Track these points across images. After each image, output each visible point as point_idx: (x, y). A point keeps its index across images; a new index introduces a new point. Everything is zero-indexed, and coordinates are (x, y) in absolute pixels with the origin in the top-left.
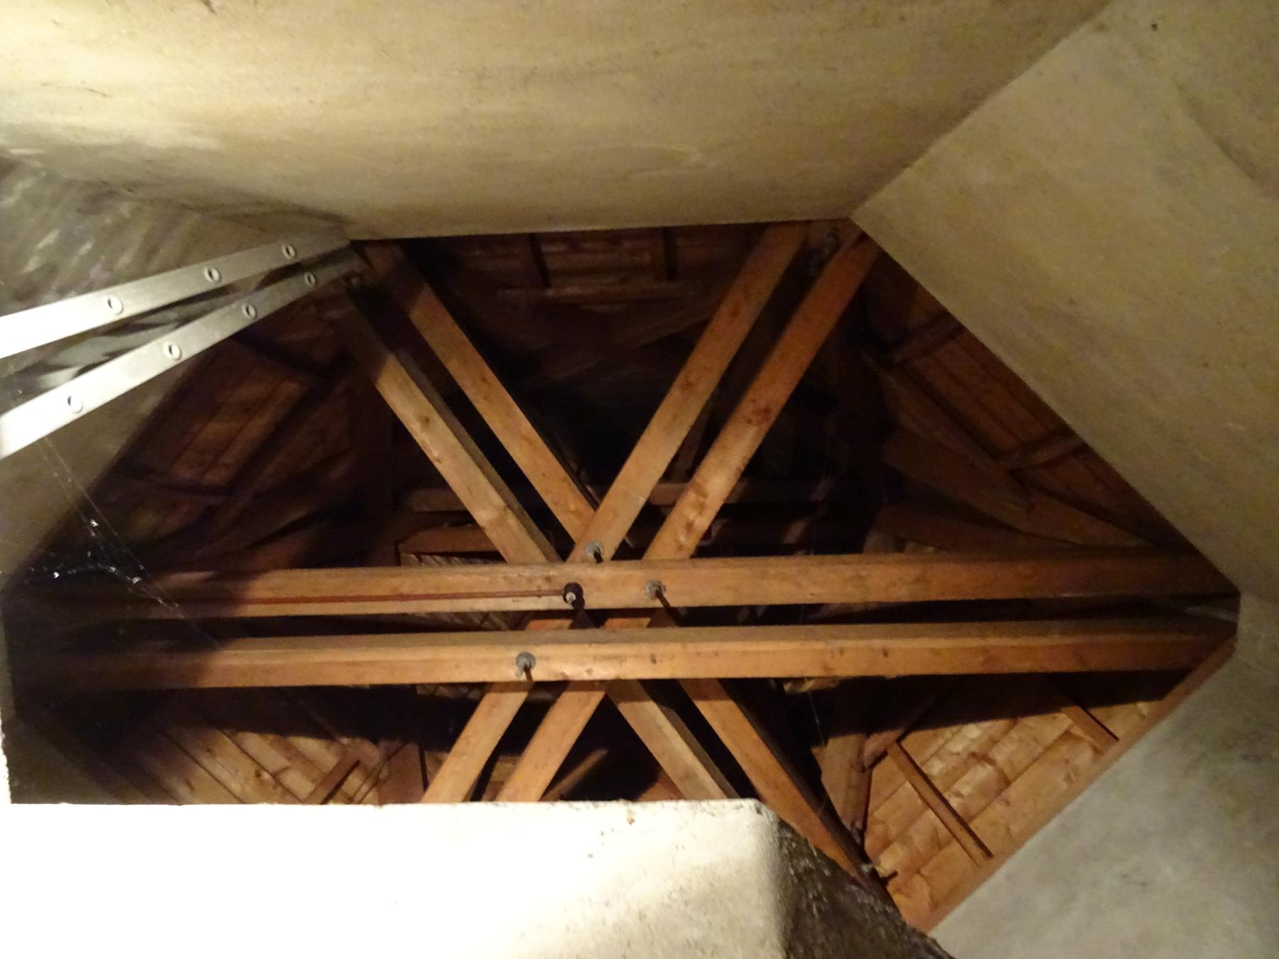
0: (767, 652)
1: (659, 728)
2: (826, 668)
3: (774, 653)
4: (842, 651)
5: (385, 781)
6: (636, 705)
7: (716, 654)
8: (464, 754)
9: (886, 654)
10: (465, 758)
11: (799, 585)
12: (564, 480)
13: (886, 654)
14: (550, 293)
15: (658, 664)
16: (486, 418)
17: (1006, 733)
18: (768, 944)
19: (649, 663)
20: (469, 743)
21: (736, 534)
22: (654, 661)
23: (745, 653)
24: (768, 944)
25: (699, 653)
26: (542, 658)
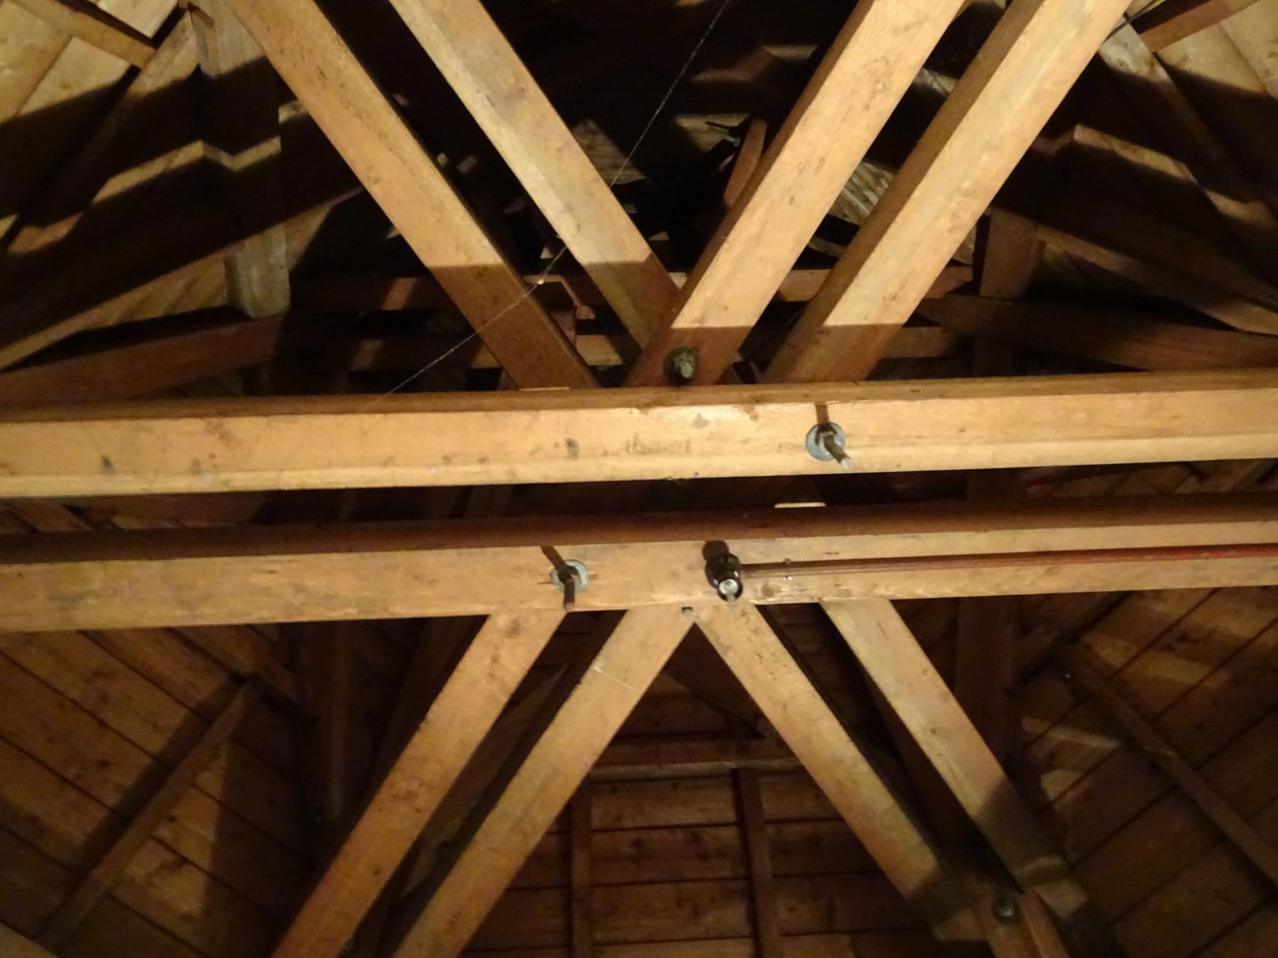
0: (347, 465)
1: (569, 208)
2: (225, 437)
3: (330, 465)
4: (196, 469)
5: (1152, 66)
6: (613, 257)
7: (447, 460)
8: (967, 194)
9: (107, 463)
10: (966, 185)
11: (300, 589)
12: (728, 648)
13: (107, 463)
14: (731, 765)
15: (562, 440)
16: (842, 734)
18: (301, 598)
19: (582, 443)
20: (954, 216)
21: (430, 649)
22: (571, 444)
23: (387, 462)
24: (299, 599)
25: (483, 461)
26: (796, 447)
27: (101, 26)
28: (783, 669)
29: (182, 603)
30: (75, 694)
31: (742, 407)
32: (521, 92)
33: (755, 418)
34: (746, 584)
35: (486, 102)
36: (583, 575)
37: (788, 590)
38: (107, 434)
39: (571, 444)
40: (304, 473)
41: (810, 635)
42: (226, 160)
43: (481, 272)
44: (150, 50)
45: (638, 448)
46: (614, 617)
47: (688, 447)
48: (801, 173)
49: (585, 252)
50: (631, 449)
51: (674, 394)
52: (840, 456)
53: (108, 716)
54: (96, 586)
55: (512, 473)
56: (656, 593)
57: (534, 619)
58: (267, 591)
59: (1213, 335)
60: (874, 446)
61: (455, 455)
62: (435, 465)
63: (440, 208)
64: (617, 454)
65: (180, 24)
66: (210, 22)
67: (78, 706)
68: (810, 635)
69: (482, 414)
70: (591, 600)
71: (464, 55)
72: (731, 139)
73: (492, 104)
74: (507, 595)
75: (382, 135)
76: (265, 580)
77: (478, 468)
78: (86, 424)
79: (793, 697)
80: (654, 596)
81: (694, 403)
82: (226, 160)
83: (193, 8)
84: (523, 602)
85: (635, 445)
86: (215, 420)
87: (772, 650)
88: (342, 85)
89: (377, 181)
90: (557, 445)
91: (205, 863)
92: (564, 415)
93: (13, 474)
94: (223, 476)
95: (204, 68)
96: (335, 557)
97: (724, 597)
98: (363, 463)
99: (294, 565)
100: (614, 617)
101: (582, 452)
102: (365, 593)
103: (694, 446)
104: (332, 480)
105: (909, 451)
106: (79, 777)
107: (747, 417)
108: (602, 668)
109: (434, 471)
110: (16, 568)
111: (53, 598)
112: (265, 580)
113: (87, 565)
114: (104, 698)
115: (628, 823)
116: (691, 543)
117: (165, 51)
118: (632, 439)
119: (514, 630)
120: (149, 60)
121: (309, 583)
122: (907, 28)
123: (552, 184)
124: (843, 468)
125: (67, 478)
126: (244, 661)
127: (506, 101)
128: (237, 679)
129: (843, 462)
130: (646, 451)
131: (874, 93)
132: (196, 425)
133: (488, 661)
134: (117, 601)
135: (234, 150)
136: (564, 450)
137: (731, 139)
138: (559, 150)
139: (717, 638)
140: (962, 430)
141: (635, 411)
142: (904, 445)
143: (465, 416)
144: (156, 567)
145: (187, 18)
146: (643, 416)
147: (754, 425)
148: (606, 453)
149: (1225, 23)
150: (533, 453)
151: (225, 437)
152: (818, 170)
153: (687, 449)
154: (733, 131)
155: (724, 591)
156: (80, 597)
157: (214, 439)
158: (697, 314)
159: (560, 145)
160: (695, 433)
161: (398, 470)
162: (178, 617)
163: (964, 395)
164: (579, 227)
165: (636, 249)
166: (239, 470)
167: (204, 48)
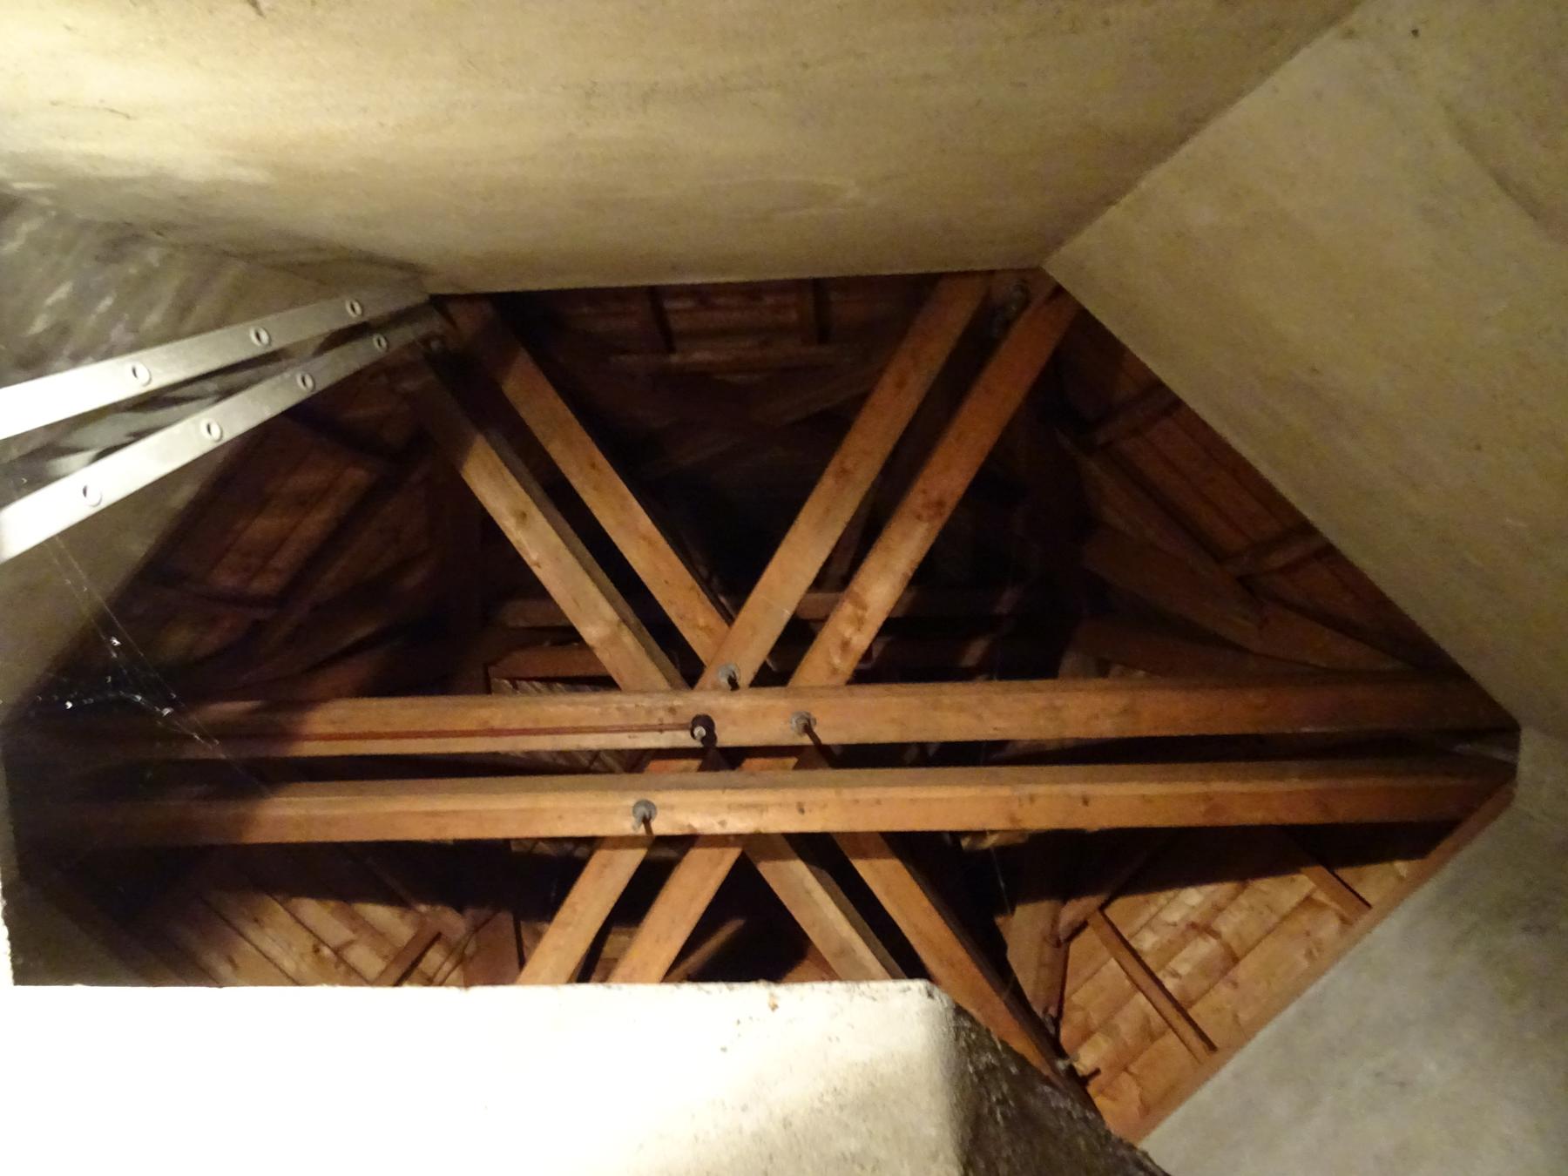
0: (940, 800)
1: (808, 892)
2: (1013, 819)
3: (949, 800)
4: (1032, 799)
6: (780, 864)
7: (878, 802)
8: (569, 924)
9: (1086, 802)
10: (570, 929)
11: (979, 717)
12: (692, 588)
13: (1086, 802)
14: (675, 359)
15: (807, 814)
16: (596, 513)
17: (1233, 898)
19: (796, 813)
20: (575, 911)
21: (902, 655)
22: (802, 811)
23: (913, 801)
25: (857, 801)
26: (664, 807)
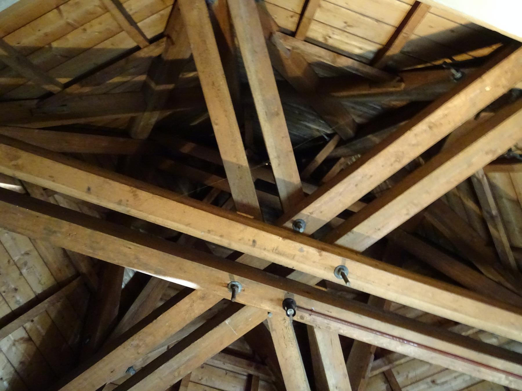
0: (174, 221)
1: (278, 157)
2: (135, 195)
3: (167, 218)
4: (120, 203)
7: (209, 232)
9: (89, 189)
12: (275, 330)
13: (89, 189)
19: (258, 243)
22: (254, 241)
23: (188, 225)
25: (221, 236)
27: (136, 31)
28: (291, 345)
29: (91, 247)
30: (16, 259)
31: (317, 250)
32: (278, 114)
33: (321, 255)
34: (297, 312)
35: (265, 113)
36: (240, 289)
37: (307, 319)
38: (94, 180)
39: (254, 241)
40: (157, 218)
41: (304, 335)
42: (153, 85)
43: (240, 167)
44: (147, 44)
45: (277, 251)
46: (243, 306)
47: (294, 257)
48: (363, 177)
49: (278, 173)
50: (274, 251)
51: (294, 236)
52: (346, 281)
53: (24, 271)
54: (63, 230)
55: (230, 244)
56: (260, 304)
57: (211, 296)
58: (125, 255)
59: (475, 273)
60: (357, 279)
61: (213, 231)
62: (204, 232)
63: (235, 141)
64: (268, 251)
65: (161, 40)
66: (173, 43)
67: (15, 264)
68: (304, 335)
69: (228, 220)
70: (239, 300)
71: (263, 96)
72: (326, 137)
73: (266, 115)
74: (203, 285)
75: (225, 111)
76: (126, 250)
77: (219, 238)
78: (88, 173)
79: (291, 357)
80: (262, 305)
81: (301, 242)
82: (153, 85)
83: (169, 37)
84: (215, 291)
85: (276, 250)
86: (134, 189)
87: (289, 336)
88: (218, 90)
89: (217, 124)
90: (249, 240)
91: (38, 343)
92: (256, 231)
93: (54, 181)
94: (128, 209)
95: (163, 56)
96: (155, 251)
97: (288, 315)
98: (179, 222)
99: (138, 248)
100: (240, 306)
101: (257, 246)
102: (159, 267)
103: (296, 258)
104: (166, 224)
105: (367, 285)
106: (4, 292)
107: (318, 254)
108: (229, 323)
109: (203, 233)
110: (38, 214)
111: (45, 229)
112: (126, 250)
113: (64, 222)
114: (25, 264)
115: (203, 382)
116: (282, 291)
117: (152, 47)
118: (276, 247)
119: (203, 298)
120: (146, 47)
121: (141, 257)
122: (413, 145)
123: (276, 147)
124: (348, 285)
125: (73, 190)
126: (84, 268)
127: (271, 115)
128: (78, 274)
129: (348, 283)
130: (279, 254)
131: (396, 161)
132: (127, 188)
133: (188, 306)
134: (69, 238)
135: (157, 83)
136: (251, 243)
137: (326, 137)
138: (283, 137)
139: (272, 325)
140: (389, 285)
141: (281, 238)
142: (367, 283)
143: (222, 219)
144: (89, 231)
145: (165, 39)
146: (283, 241)
147: (319, 258)
148: (265, 249)
149: (511, 174)
150: (240, 240)
151: (135, 195)
152: (369, 179)
153: (293, 257)
154: (328, 135)
155: (288, 313)
156: (55, 232)
157: (131, 195)
158: (311, 211)
159: (283, 136)
160: (298, 253)
161: (190, 229)
162: (88, 252)
163: (393, 273)
164: (279, 165)
165: (295, 179)
166: (134, 209)
167: (166, 50)
